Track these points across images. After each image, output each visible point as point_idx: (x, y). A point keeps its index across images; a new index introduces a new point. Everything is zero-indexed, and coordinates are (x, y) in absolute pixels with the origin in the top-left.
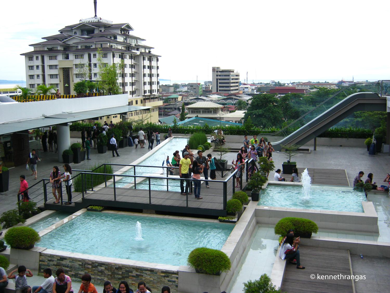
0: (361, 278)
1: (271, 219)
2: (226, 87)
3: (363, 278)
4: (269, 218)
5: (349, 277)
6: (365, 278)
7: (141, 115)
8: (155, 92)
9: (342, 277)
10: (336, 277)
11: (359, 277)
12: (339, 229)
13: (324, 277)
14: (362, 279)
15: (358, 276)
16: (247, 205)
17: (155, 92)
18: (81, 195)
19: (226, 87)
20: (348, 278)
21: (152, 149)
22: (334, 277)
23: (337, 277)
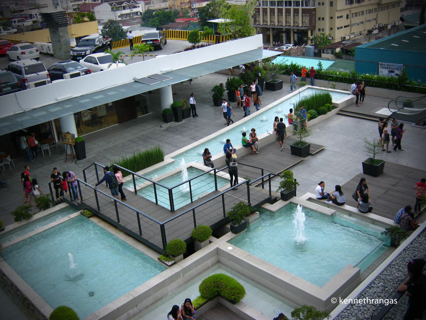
0: (391, 302)
1: (230, 262)
2: (177, 35)
3: (394, 302)
4: (229, 260)
5: (378, 301)
6: (396, 302)
7: (376, 13)
8: (213, 40)
9: (369, 301)
10: (362, 301)
11: (389, 301)
12: (272, 290)
13: (347, 301)
14: (393, 303)
15: (388, 300)
16: (218, 238)
17: (213, 40)
18: (302, 140)
19: (177, 35)
20: (377, 302)
21: (228, 125)
22: (359, 301)
23: (363, 300)
